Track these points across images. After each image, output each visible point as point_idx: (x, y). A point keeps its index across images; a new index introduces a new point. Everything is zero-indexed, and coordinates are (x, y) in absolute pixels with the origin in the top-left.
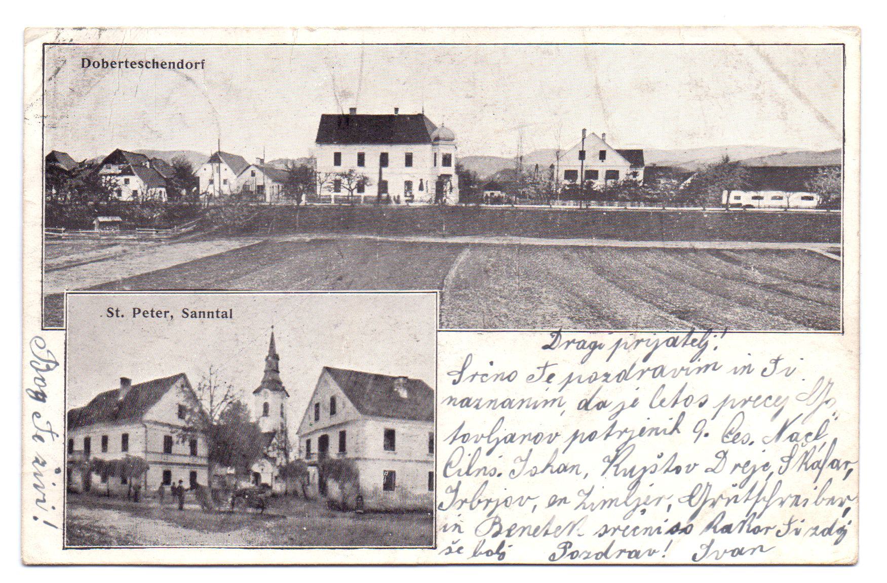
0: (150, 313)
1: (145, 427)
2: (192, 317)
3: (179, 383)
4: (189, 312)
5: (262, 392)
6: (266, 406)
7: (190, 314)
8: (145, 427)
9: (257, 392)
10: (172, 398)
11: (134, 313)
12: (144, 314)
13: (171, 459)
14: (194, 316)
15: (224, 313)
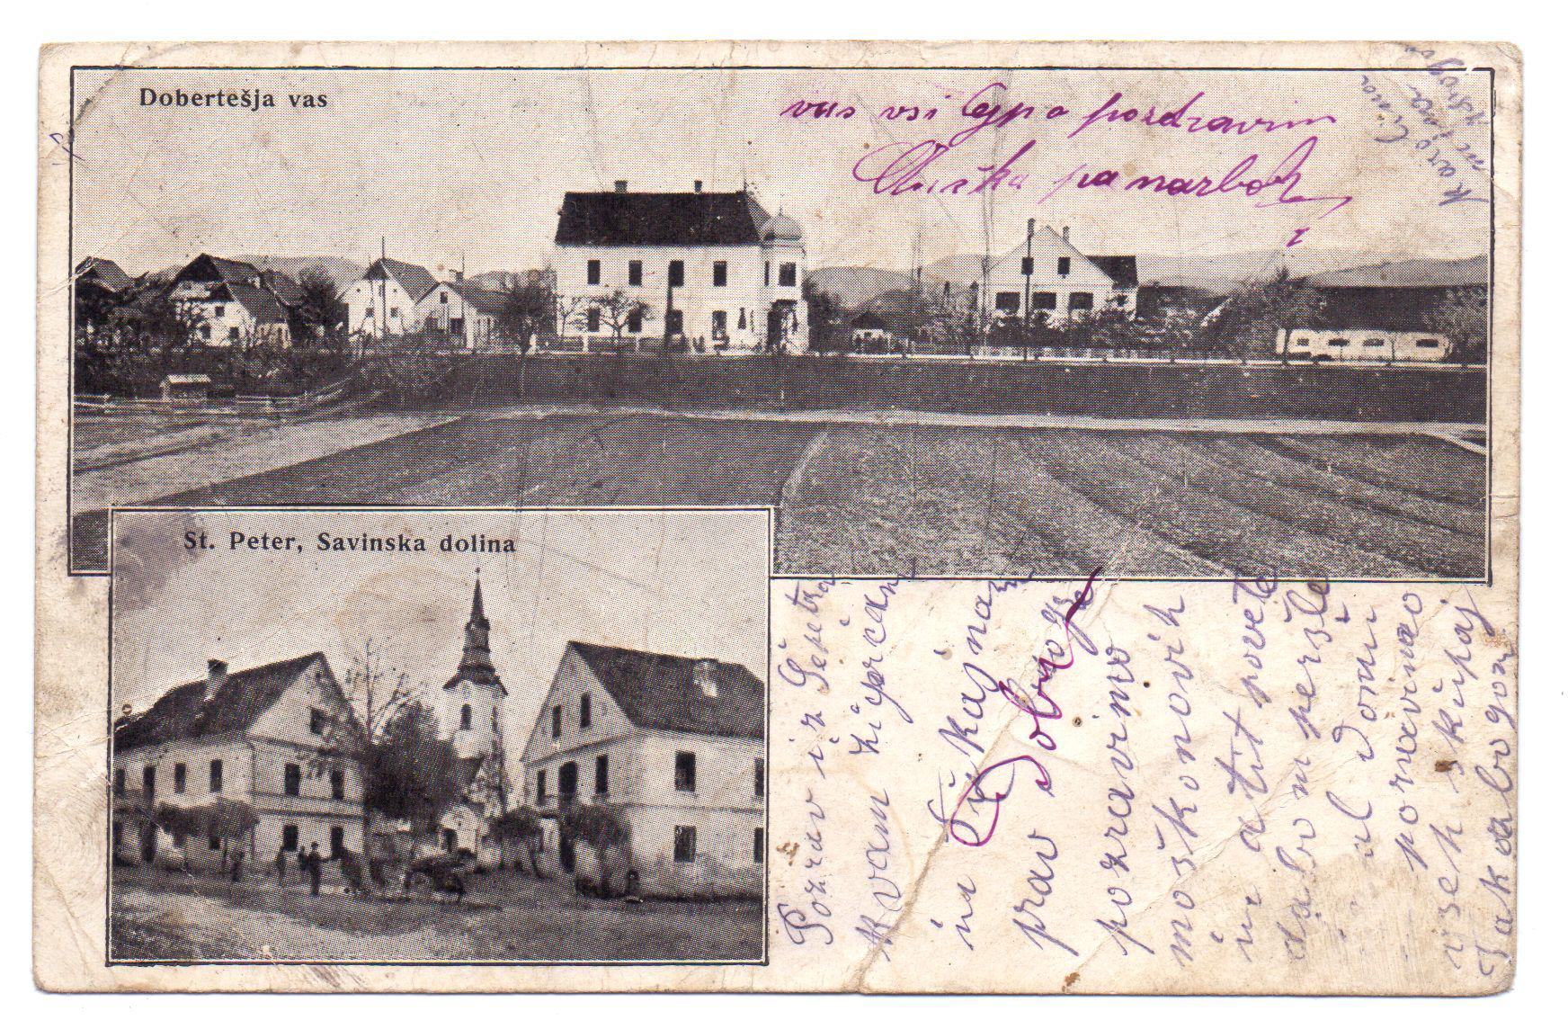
0: (261, 541)
1: (252, 747)
2: (335, 548)
3: (311, 670)
4: (330, 540)
5: (459, 687)
6: (466, 711)
7: (332, 544)
8: (252, 747)
9: (450, 685)
10: (301, 696)
11: (233, 543)
12: (250, 543)
13: (297, 805)
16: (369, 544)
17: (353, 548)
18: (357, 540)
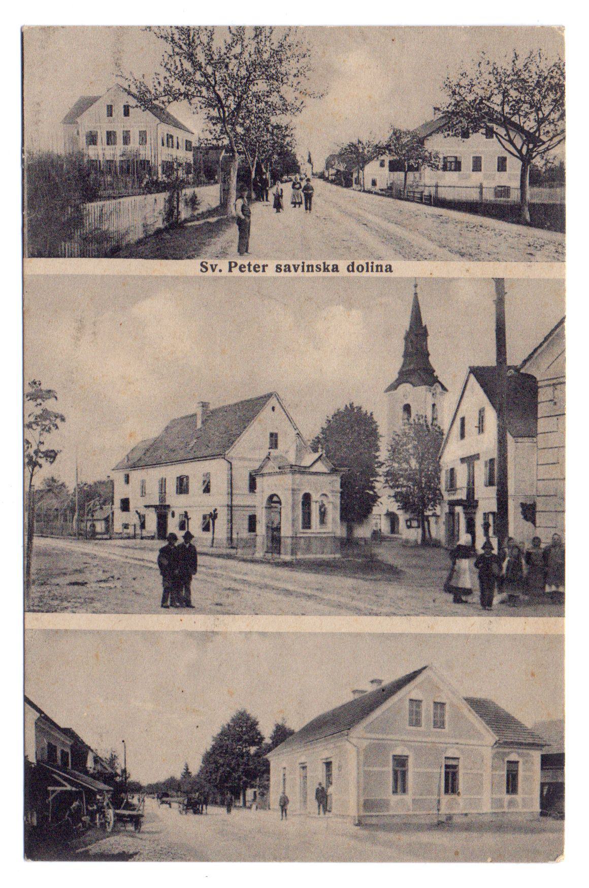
0: (247, 267)
14: (388, 270)
15: (388, 267)
16: (306, 268)
17: (296, 271)
18: (299, 266)
